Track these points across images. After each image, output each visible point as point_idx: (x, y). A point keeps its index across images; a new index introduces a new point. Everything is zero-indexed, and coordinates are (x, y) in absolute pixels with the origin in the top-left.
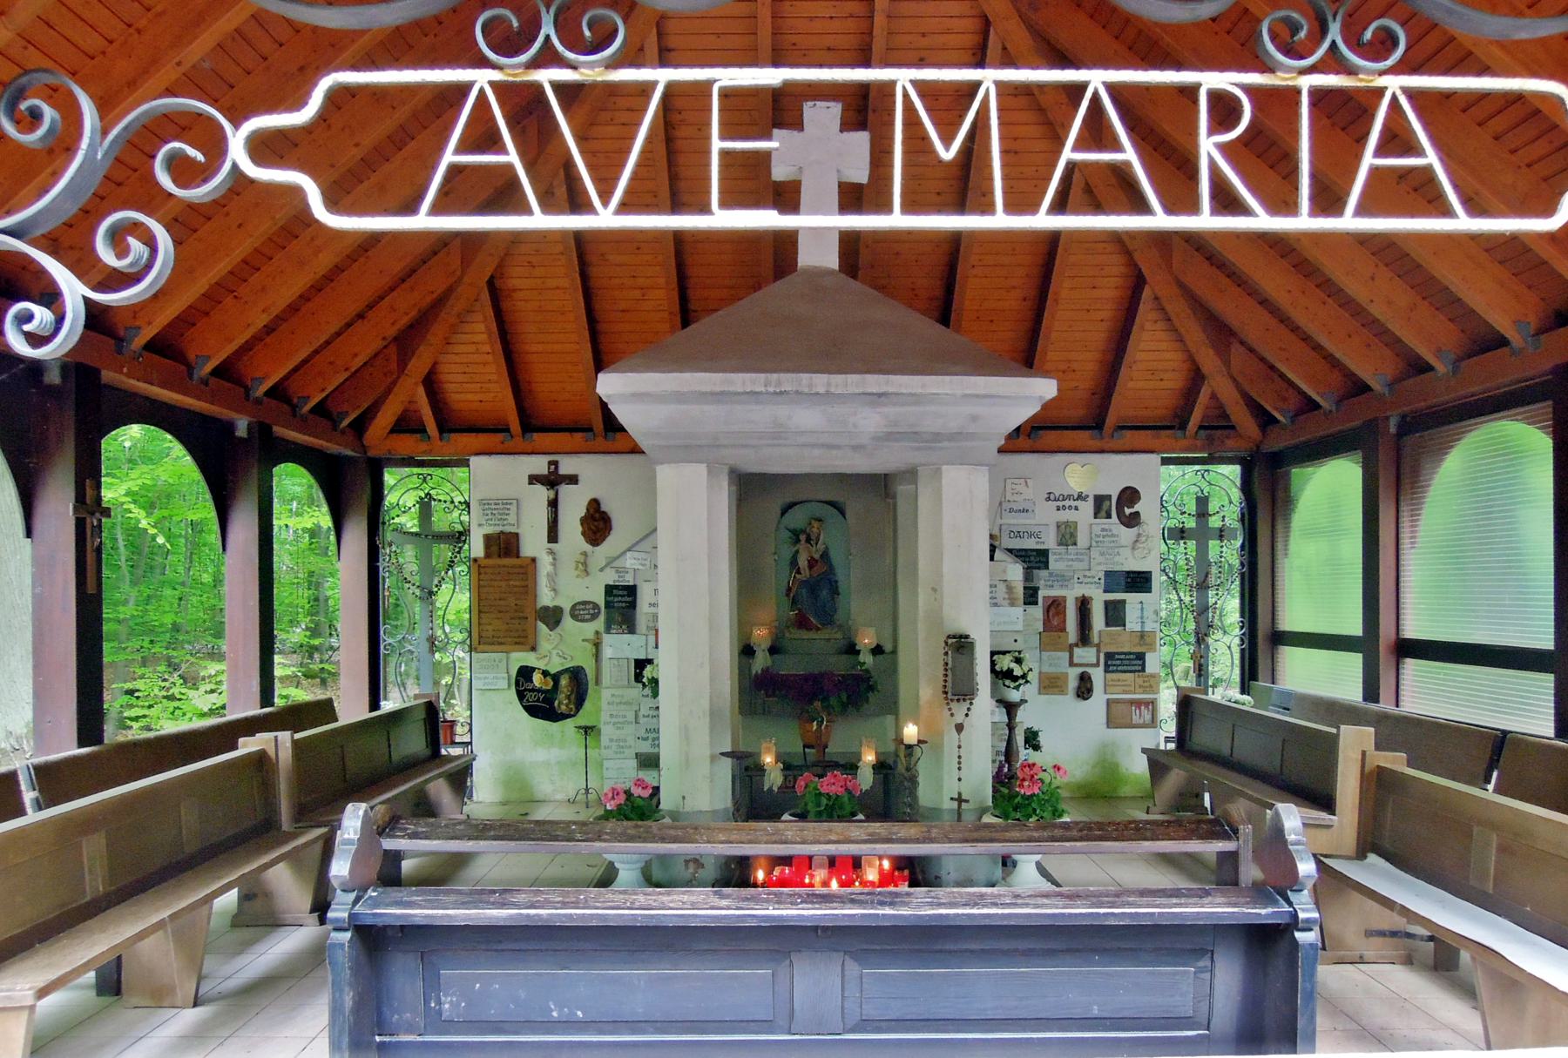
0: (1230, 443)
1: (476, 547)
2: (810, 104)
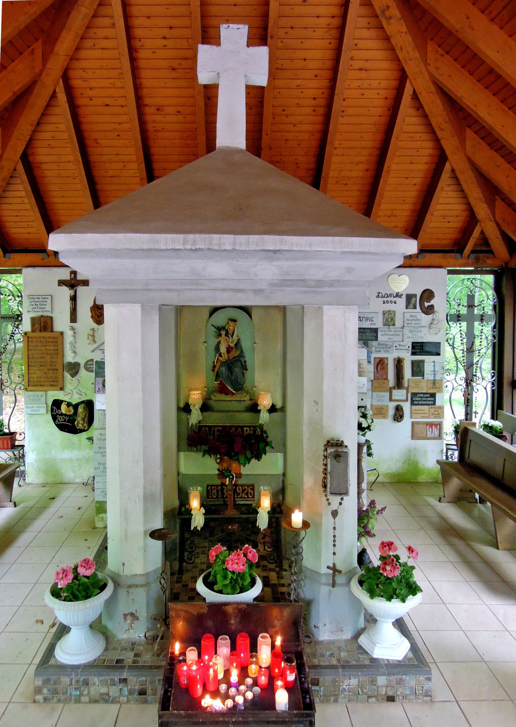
0: (489, 261)
1: (26, 326)
2: (225, 26)
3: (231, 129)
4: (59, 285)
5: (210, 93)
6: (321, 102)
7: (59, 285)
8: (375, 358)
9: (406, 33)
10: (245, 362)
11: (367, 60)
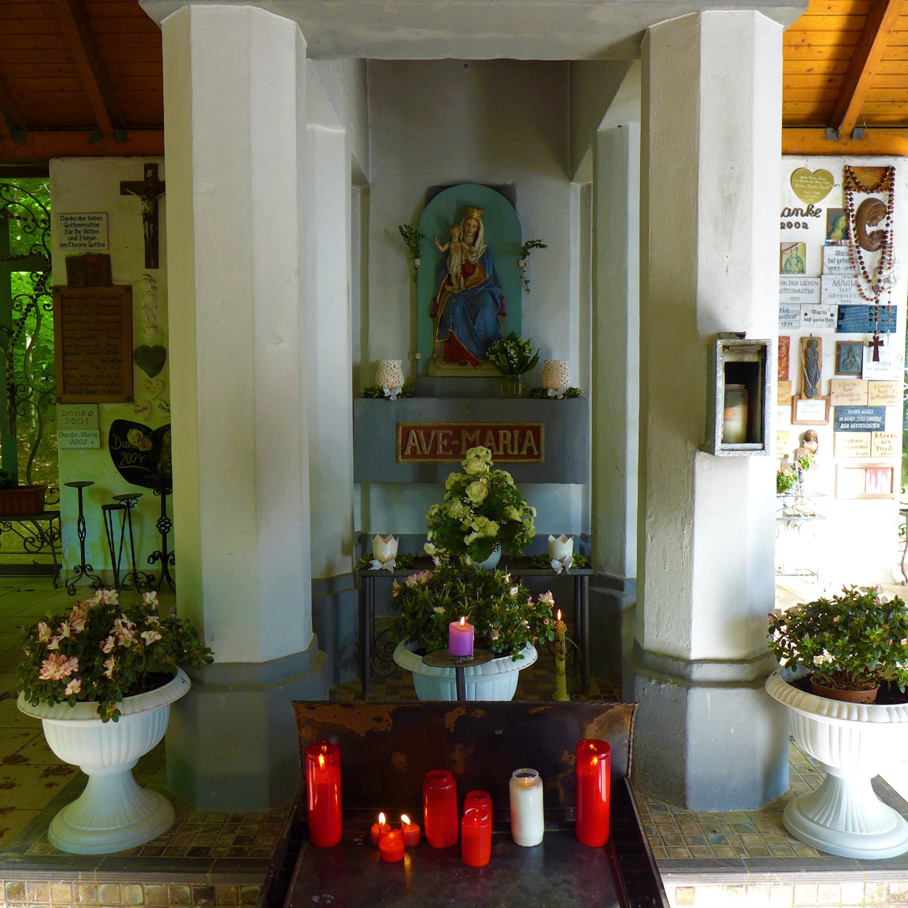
1: (59, 276)
4: (123, 192)
7: (123, 192)
10: (502, 298)
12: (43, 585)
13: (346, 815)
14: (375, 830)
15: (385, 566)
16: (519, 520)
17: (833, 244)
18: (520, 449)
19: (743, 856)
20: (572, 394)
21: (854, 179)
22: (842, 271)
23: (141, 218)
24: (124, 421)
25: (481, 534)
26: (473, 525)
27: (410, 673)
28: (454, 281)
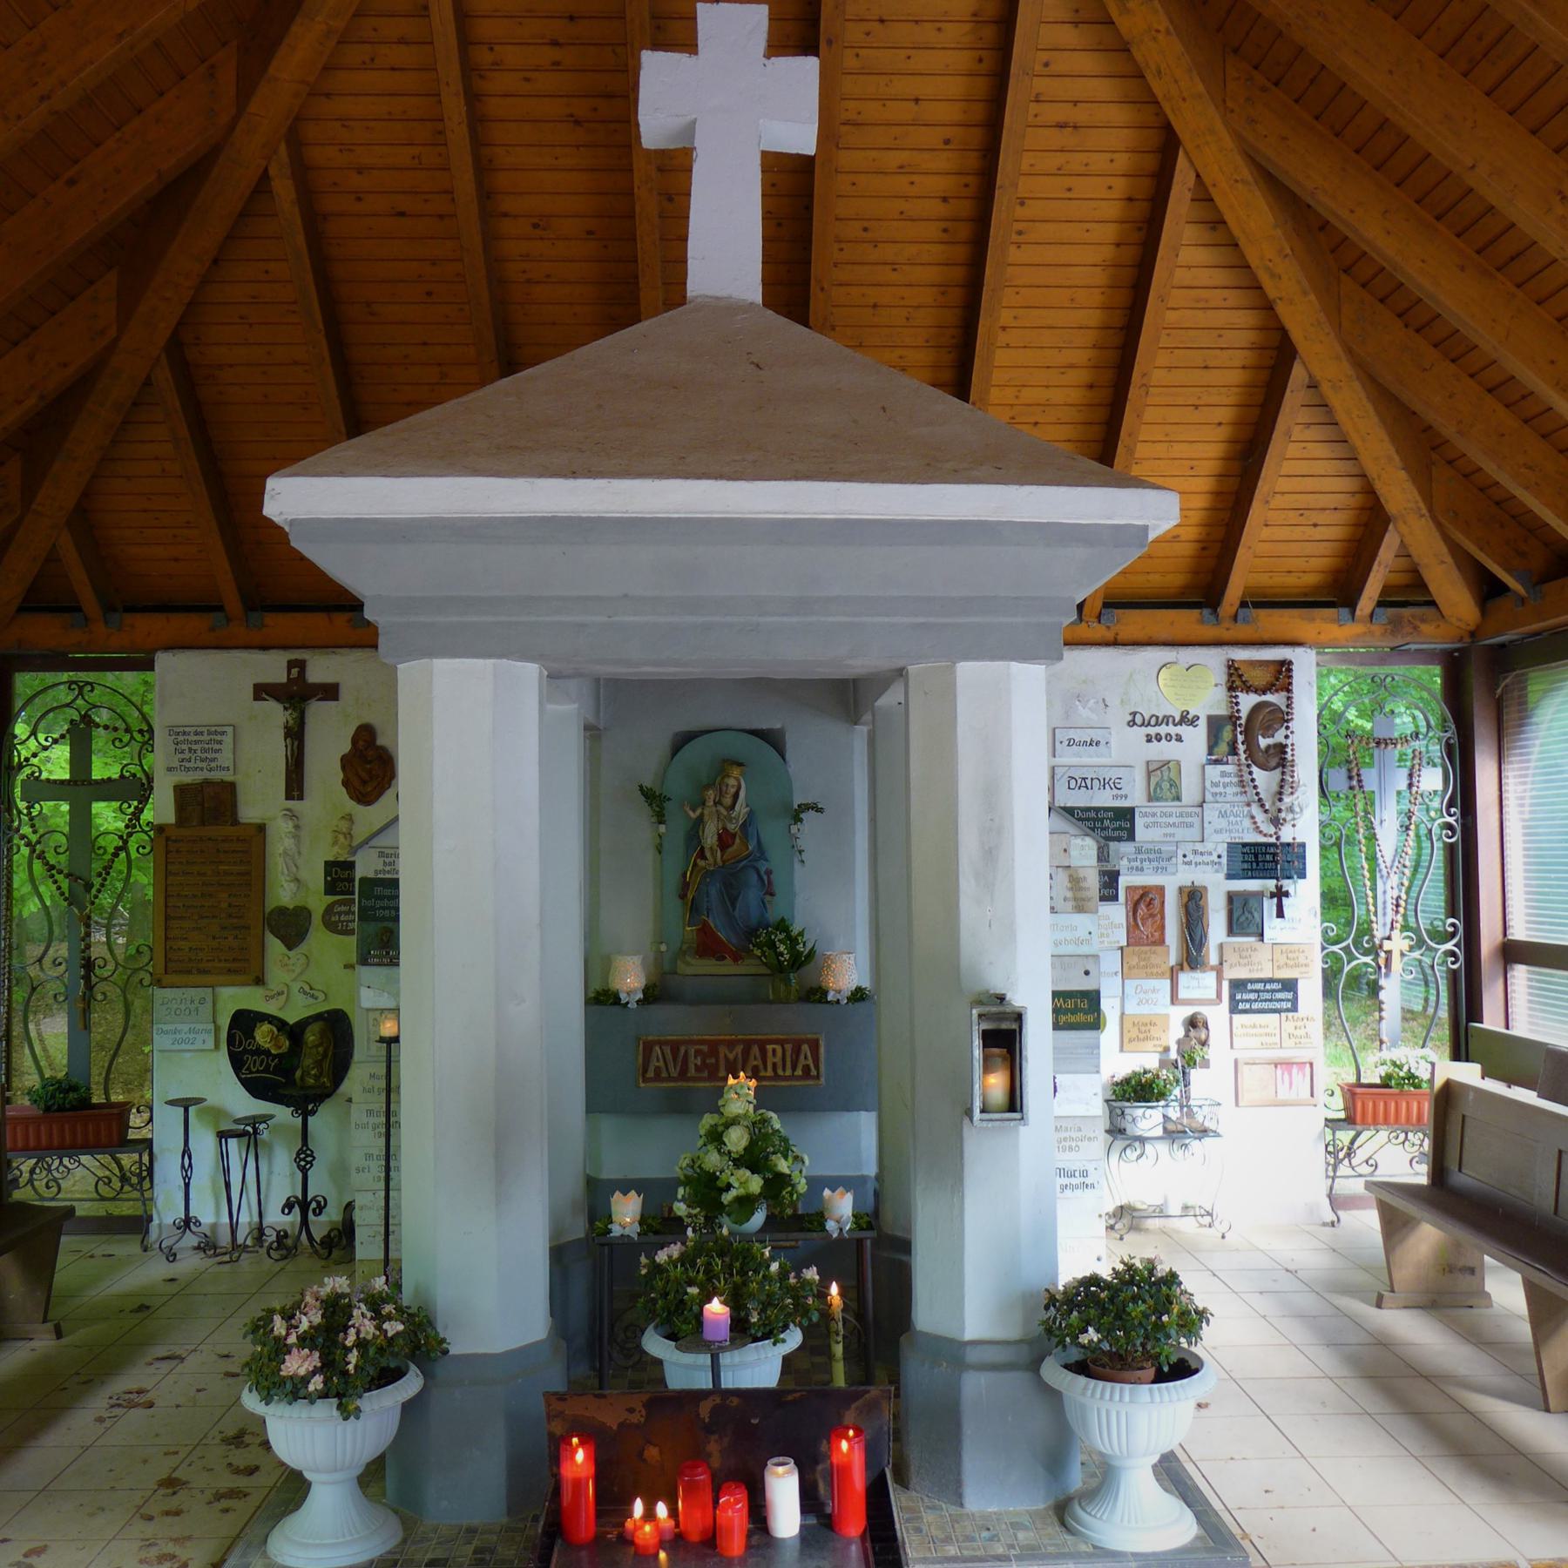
1: (160, 809)
3: (725, 247)
4: (257, 697)
5: (675, 167)
6: (965, 208)
7: (257, 697)
8: (1128, 888)
9: (1168, 32)
10: (769, 873)
11: (1075, 103)
12: (126, 1247)
13: (599, 1514)
14: (629, 1524)
15: (627, 1232)
16: (787, 1171)
17: (1217, 762)
18: (794, 1068)
19: (1013, 1552)
20: (858, 995)
21: (1240, 676)
22: (1230, 798)
23: (281, 733)
24: (250, 1012)
25: (742, 1191)
26: (732, 1180)
27: (659, 1363)
28: (708, 854)
